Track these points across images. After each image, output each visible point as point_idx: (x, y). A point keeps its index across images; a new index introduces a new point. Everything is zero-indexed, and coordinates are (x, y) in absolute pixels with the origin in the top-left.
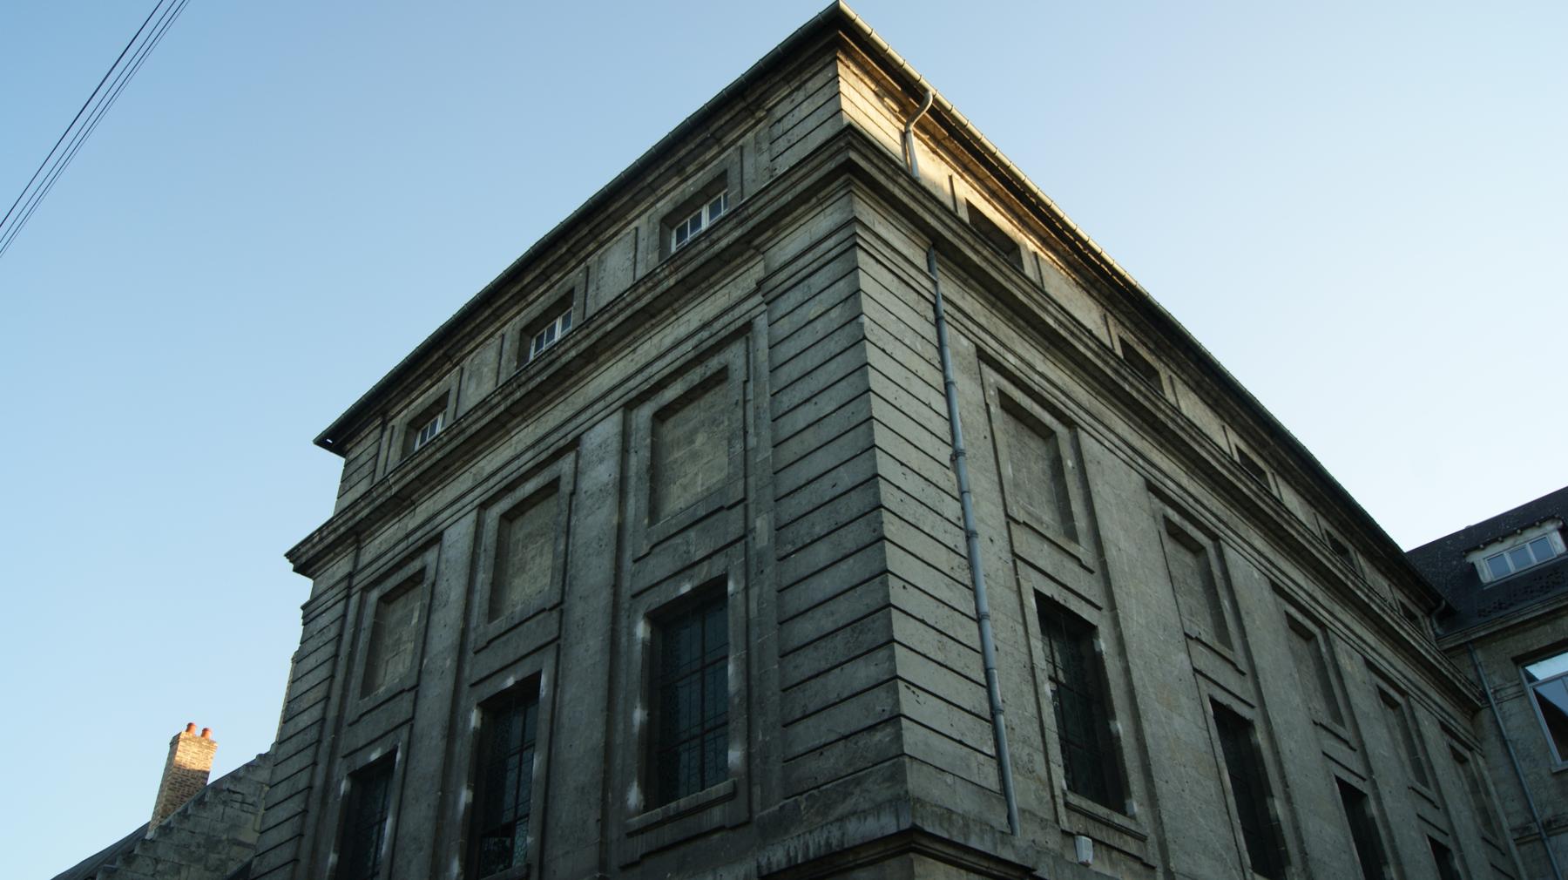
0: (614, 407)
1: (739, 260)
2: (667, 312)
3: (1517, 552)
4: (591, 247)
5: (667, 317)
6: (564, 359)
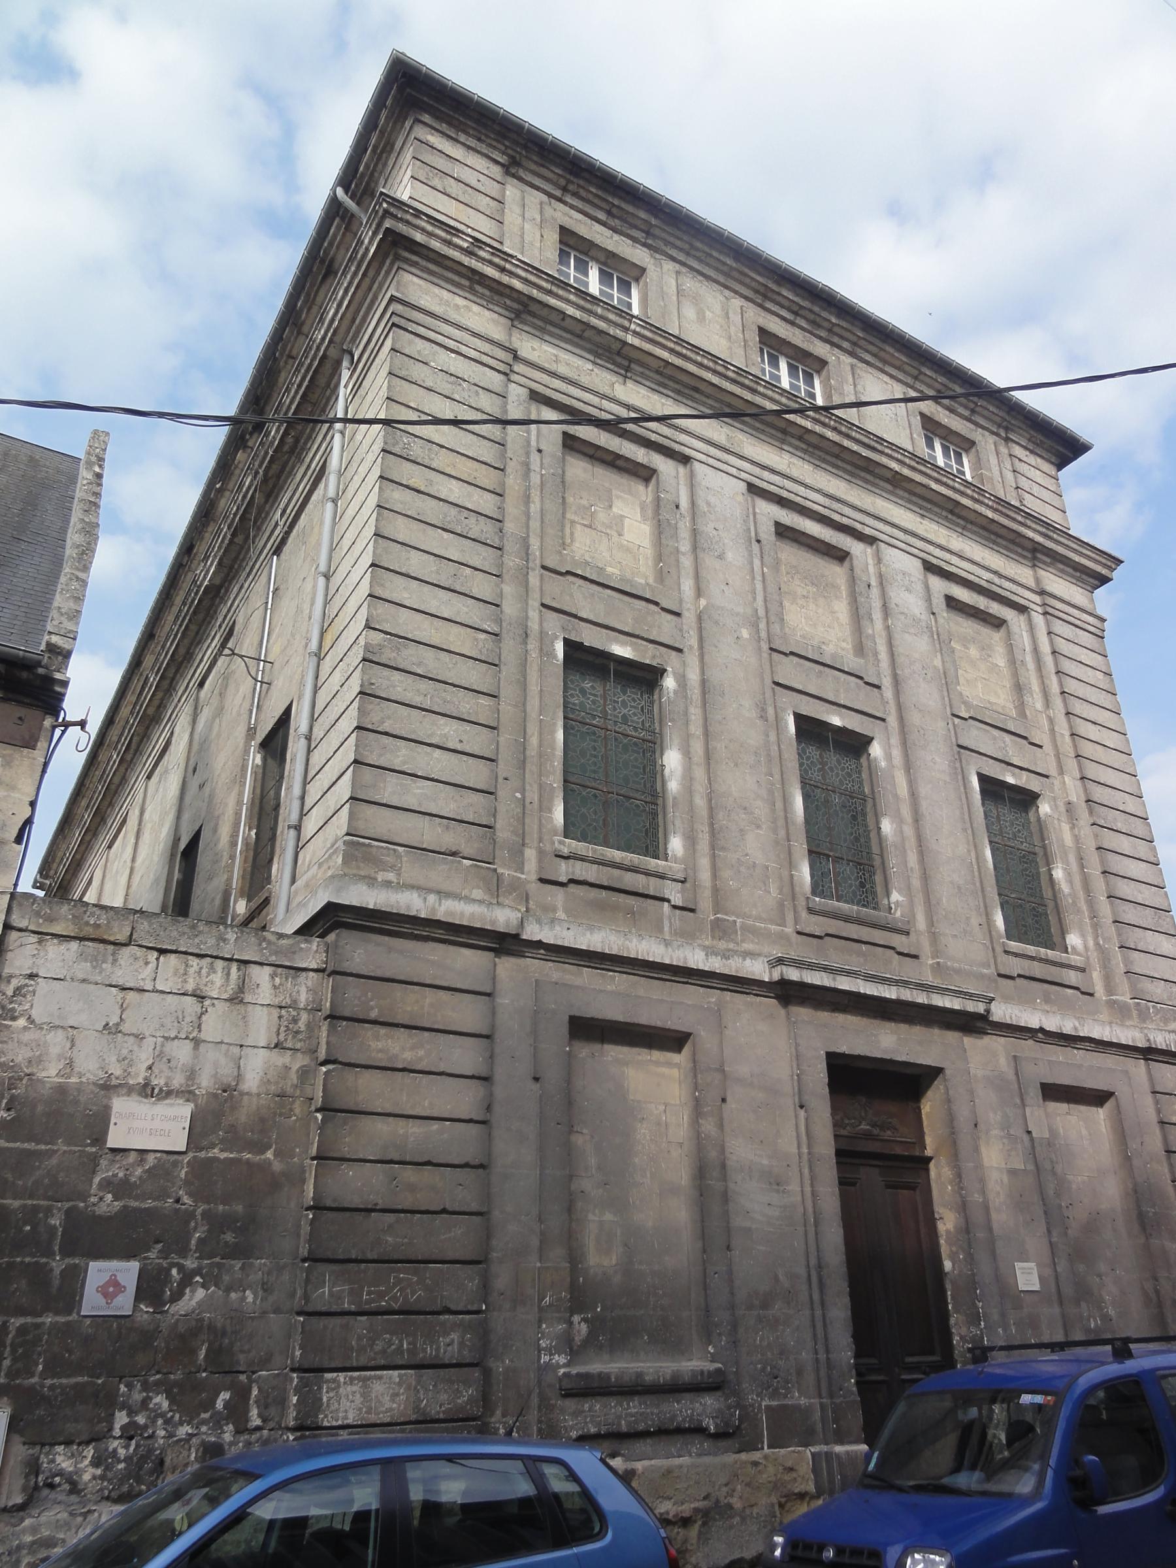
0: (743, 475)
1: (1020, 550)
2: (962, 522)
3: (594, 851)
4: (845, 345)
5: (958, 525)
6: (884, 460)
